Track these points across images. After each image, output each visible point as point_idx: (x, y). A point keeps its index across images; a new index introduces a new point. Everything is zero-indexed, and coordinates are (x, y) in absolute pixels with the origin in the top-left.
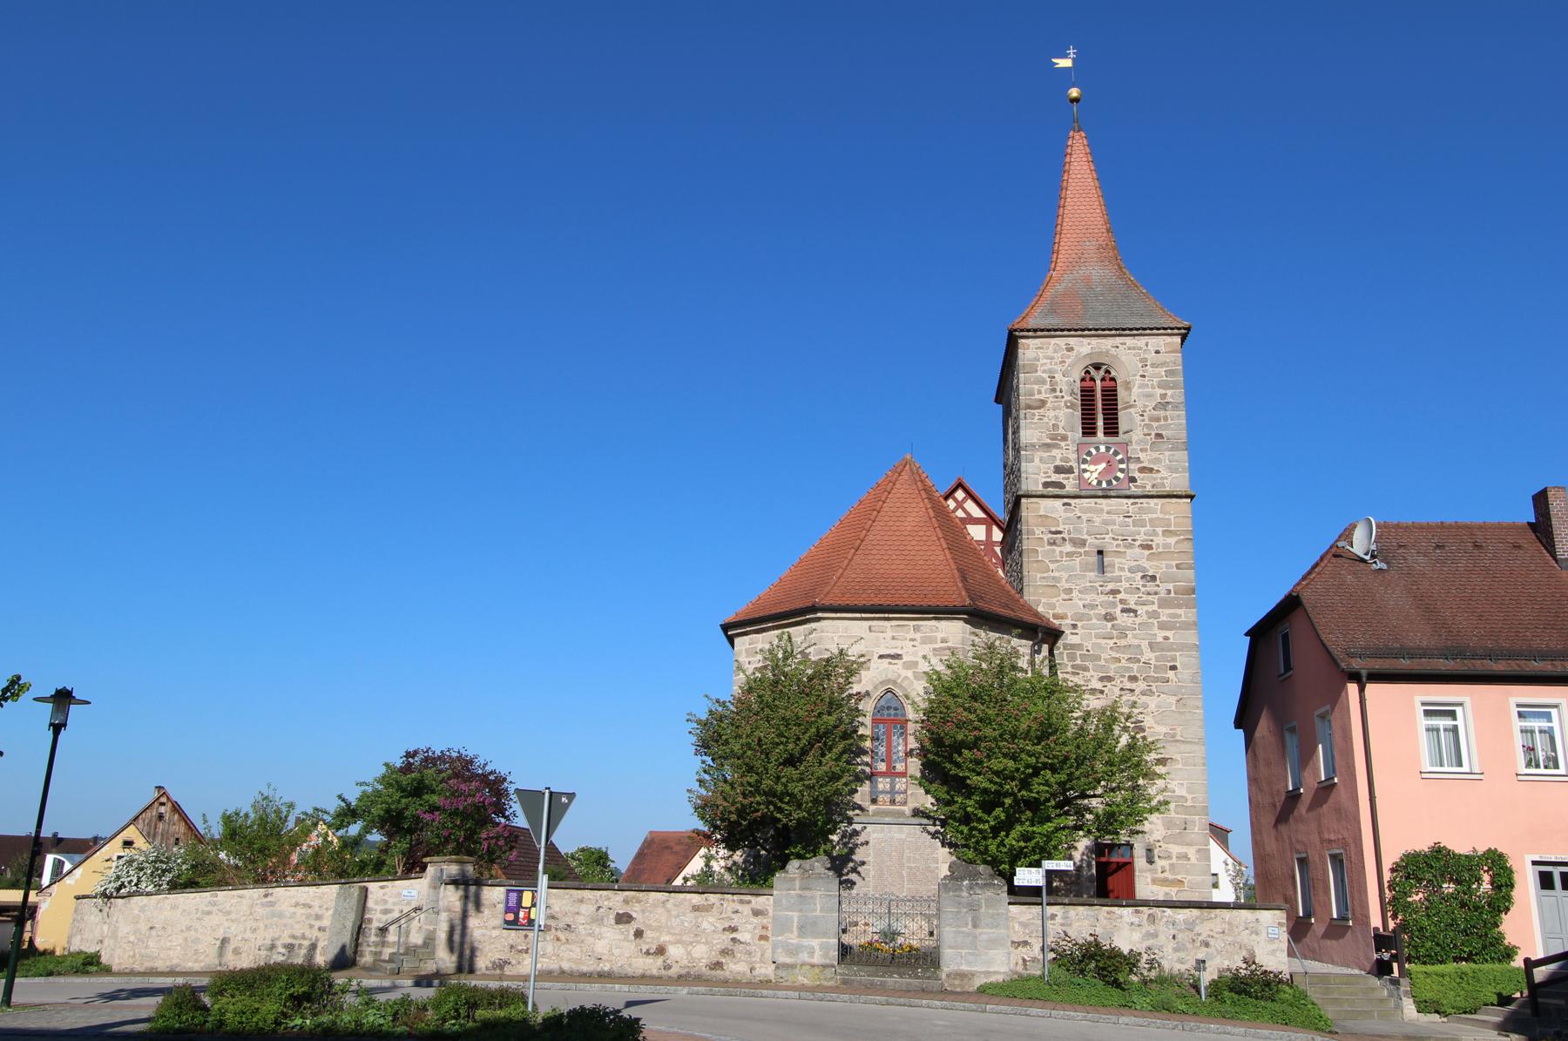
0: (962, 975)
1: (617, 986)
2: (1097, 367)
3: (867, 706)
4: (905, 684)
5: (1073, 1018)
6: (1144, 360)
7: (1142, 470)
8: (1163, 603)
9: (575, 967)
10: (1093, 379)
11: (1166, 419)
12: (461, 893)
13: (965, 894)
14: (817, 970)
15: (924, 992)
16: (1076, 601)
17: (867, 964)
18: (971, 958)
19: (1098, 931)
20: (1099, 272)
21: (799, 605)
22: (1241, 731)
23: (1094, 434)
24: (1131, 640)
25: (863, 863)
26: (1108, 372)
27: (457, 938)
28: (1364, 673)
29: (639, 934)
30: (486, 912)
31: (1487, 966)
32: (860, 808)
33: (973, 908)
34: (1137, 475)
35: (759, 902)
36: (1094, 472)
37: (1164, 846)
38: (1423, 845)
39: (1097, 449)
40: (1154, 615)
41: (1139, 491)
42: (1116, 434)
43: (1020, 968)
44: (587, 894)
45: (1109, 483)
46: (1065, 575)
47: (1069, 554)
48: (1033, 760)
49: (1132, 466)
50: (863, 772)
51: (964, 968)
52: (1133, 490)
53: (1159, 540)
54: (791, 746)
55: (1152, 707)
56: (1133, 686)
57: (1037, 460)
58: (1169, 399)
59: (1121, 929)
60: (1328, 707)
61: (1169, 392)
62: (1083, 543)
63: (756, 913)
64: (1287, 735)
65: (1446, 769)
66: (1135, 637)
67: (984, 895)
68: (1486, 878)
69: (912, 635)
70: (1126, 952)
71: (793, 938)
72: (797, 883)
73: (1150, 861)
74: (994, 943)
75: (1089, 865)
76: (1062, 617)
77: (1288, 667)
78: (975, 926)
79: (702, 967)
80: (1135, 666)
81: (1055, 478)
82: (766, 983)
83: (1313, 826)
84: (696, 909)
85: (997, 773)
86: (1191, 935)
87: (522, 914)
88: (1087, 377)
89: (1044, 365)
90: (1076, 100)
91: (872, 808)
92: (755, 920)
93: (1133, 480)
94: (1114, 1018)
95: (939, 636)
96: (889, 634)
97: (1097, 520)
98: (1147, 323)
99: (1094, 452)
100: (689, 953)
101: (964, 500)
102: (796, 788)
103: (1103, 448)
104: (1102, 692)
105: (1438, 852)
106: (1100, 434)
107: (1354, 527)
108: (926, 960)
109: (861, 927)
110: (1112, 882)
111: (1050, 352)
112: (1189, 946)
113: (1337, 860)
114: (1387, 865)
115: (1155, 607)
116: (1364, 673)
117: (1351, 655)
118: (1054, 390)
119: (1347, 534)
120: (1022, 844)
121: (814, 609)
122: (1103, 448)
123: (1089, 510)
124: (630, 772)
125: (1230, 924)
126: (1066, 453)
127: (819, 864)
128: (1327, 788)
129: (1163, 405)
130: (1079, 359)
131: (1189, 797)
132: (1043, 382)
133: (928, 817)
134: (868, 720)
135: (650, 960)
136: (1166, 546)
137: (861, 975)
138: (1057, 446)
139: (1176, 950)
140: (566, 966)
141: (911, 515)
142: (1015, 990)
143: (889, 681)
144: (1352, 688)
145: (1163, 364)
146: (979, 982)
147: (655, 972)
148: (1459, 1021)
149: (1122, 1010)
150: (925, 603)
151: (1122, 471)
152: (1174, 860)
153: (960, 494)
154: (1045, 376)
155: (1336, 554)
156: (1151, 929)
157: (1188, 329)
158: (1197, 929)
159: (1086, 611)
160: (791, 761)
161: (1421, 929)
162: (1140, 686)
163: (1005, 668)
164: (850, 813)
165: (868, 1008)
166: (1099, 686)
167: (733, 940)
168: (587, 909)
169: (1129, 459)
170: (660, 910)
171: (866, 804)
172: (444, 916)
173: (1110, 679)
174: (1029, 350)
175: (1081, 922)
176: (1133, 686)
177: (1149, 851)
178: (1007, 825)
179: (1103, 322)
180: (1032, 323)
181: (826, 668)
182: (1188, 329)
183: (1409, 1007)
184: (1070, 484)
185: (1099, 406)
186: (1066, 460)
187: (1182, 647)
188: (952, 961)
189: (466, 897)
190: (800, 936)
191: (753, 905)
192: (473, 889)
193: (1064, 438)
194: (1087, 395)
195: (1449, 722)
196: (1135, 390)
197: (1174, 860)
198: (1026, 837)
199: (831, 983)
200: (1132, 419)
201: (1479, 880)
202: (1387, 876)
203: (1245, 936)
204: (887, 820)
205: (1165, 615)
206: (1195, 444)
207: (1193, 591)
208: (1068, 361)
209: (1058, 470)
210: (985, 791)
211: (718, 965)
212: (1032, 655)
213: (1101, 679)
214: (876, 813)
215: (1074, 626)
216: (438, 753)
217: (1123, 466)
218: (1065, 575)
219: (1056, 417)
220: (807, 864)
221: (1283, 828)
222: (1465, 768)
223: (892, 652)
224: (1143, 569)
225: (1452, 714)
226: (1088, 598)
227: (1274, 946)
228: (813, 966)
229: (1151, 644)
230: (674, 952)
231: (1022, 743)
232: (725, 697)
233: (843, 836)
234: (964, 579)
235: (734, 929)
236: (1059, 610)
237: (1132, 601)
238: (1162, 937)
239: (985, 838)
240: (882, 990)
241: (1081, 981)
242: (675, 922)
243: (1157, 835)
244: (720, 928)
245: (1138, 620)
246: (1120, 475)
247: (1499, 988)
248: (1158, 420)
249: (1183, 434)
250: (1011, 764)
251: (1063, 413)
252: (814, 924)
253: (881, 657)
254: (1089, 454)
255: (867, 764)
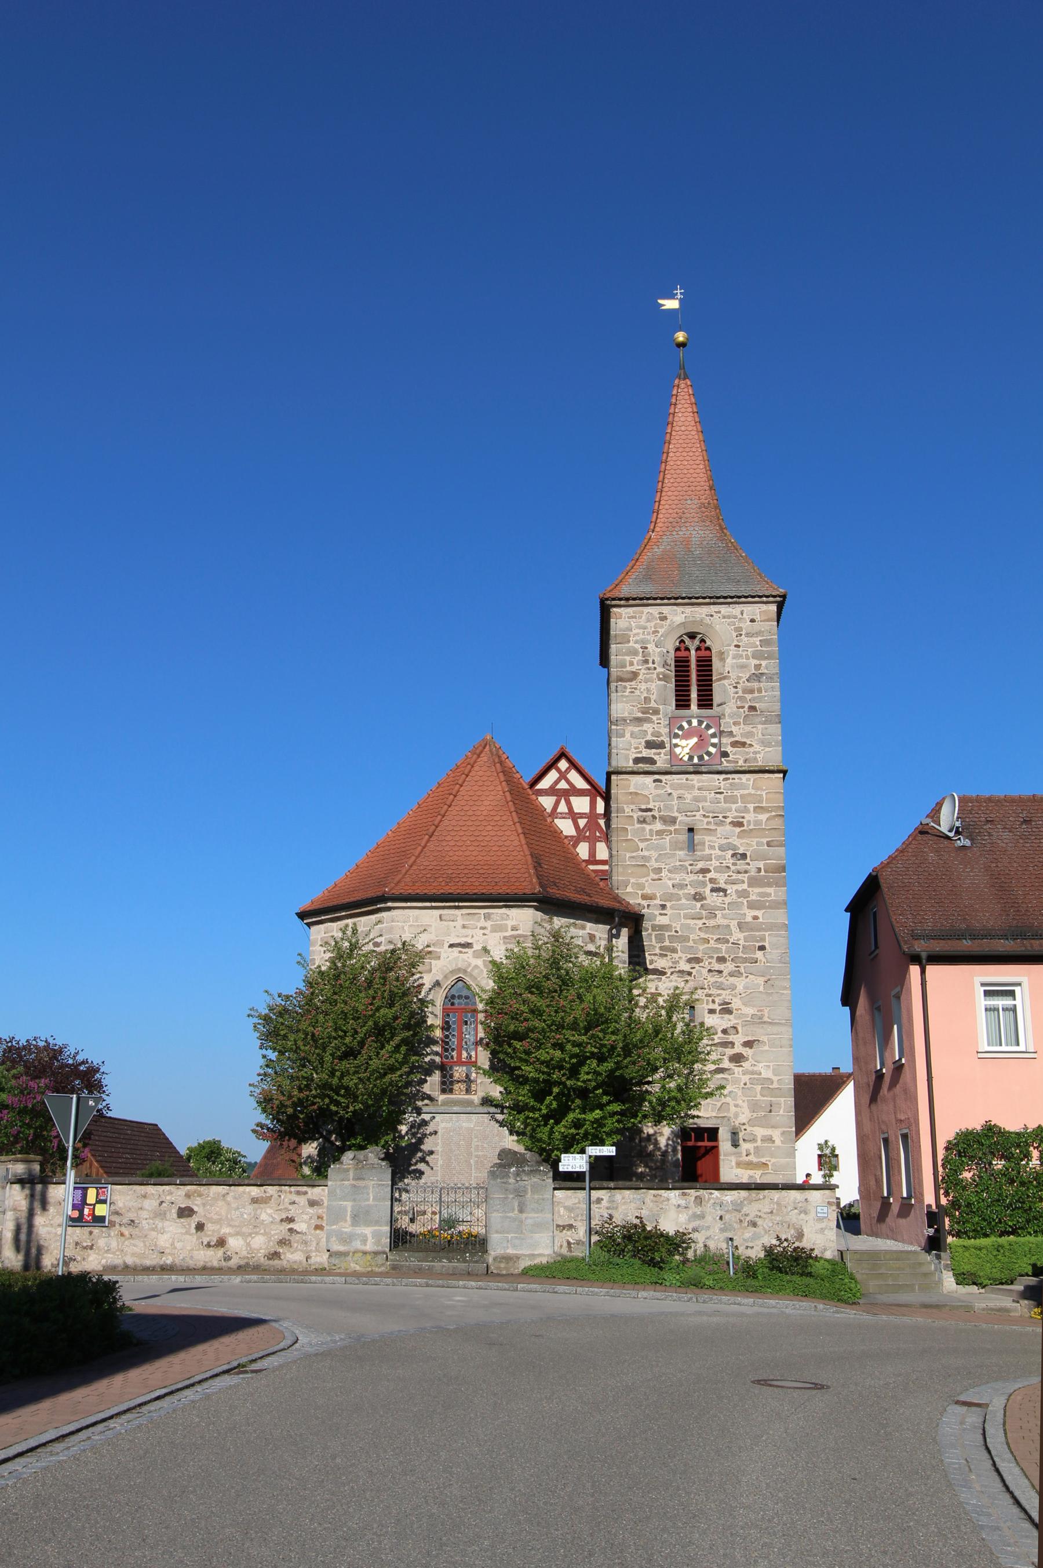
0: (508, 1259)
1: (173, 1277)
2: (692, 636)
3: (439, 998)
4: (475, 973)
5: (597, 1294)
6: (738, 630)
7: (735, 744)
8: (754, 882)
9: (138, 1261)
10: (687, 649)
11: (760, 691)
12: (27, 1191)
13: (512, 1180)
14: (369, 1257)
15: (469, 1275)
16: (665, 880)
17: (427, 1250)
18: (517, 1242)
19: (644, 1213)
20: (699, 533)
21: (370, 894)
22: (847, 1008)
23: (688, 706)
24: (720, 920)
25: (431, 1153)
26: (703, 641)
27: (23, 1237)
28: (924, 955)
29: (200, 1227)
30: (52, 1210)
31: (1028, 1238)
32: (430, 1098)
33: (520, 1194)
34: (729, 749)
35: (315, 1193)
36: (685, 747)
37: (749, 1129)
38: (976, 1124)
39: (689, 723)
40: (743, 894)
41: (730, 766)
42: (710, 706)
43: (564, 1251)
44: (150, 1189)
45: (701, 758)
46: (654, 854)
47: (660, 833)
48: (577, 1050)
49: (724, 740)
50: (433, 1061)
51: (510, 1251)
52: (725, 764)
53: (750, 817)
54: (347, 1040)
55: (740, 987)
56: (721, 967)
57: (628, 735)
58: (763, 670)
59: (669, 1210)
60: (898, 989)
61: (764, 663)
62: (673, 821)
63: (312, 1203)
64: (876, 1013)
65: (1004, 1048)
66: (724, 917)
67: (529, 1182)
68: (1035, 1154)
69: (482, 923)
70: (672, 1233)
71: (347, 1228)
72: (351, 1174)
73: (735, 1144)
74: (538, 1227)
75: (675, 1150)
76: (651, 897)
77: (876, 947)
78: (521, 1211)
79: (260, 1257)
80: (724, 947)
81: (646, 753)
82: (321, 1271)
83: (891, 1106)
84: (255, 1201)
85: (547, 1063)
86: (739, 1216)
87: (86, 1211)
88: (681, 648)
89: (636, 635)
90: (682, 345)
91: (442, 1097)
92: (311, 1210)
93: (725, 754)
94: (634, 1293)
95: (510, 923)
96: (460, 922)
97: (688, 797)
98: (743, 590)
99: (685, 725)
100: (248, 1244)
101: (568, 770)
102: (351, 1082)
103: (695, 722)
104: (690, 974)
105: (990, 1129)
106: (694, 706)
107: (944, 799)
108: (477, 1244)
109: (429, 1215)
110: (702, 1166)
111: (642, 622)
112: (736, 1226)
113: (905, 1137)
114: (941, 1145)
115: (745, 886)
116: (924, 955)
117: (916, 937)
118: (646, 662)
119: (935, 814)
120: (573, 1131)
121: (383, 899)
122: (695, 722)
123: (680, 786)
124: (192, 1063)
125: (778, 1204)
126: (657, 727)
127: (373, 1155)
128: (898, 1068)
129: (757, 677)
130: (672, 629)
131: (775, 1079)
132: (635, 653)
133: (496, 1106)
134: (438, 1010)
135: (210, 1252)
136: (757, 822)
137: (410, 1259)
138: (648, 720)
139: (722, 1230)
140: (130, 1260)
141: (487, 795)
142: (559, 1271)
143: (459, 970)
144: (914, 970)
145: (758, 633)
146: (524, 1264)
147: (215, 1264)
148: (993, 1291)
149: (803, 1299)
150: (495, 891)
151: (714, 745)
152: (759, 1143)
153: (563, 765)
154: (638, 646)
155: (923, 831)
156: (698, 1211)
157: (784, 597)
158: (745, 1210)
159: (676, 891)
160: (350, 1053)
161: (969, 1205)
162: (728, 967)
163: (559, 953)
164: (419, 1103)
165: (415, 1291)
166: (686, 967)
167: (291, 1230)
168: (150, 1204)
169: (721, 732)
170: (220, 1203)
171: (436, 1093)
172: (10, 1215)
173: (698, 960)
174: (622, 619)
175: (625, 1206)
176: (721, 967)
177: (734, 1134)
178: (558, 1115)
179: (698, 589)
180: (625, 590)
181: (390, 962)
182: (784, 597)
183: (949, 1281)
184: (662, 760)
185: (693, 677)
186: (657, 734)
187: (771, 927)
188: (499, 1246)
189: (32, 1196)
190: (353, 1225)
191: (309, 1196)
192: (39, 1187)
193: (656, 712)
194: (681, 665)
195: (1008, 1002)
196: (729, 661)
197: (759, 1143)
198: (577, 1124)
199: (383, 1269)
200: (725, 691)
201: (1027, 1156)
202: (941, 1154)
203: (794, 1217)
204: (455, 1109)
205: (755, 894)
206: (787, 718)
207: (783, 869)
208: (661, 631)
209: (650, 745)
210: (536, 1081)
211: (276, 1255)
212: (610, 940)
213: (689, 961)
214: (445, 1103)
215: (663, 907)
216: (23, 1042)
217: (715, 740)
218: (654, 854)
219: (648, 690)
220: (361, 1154)
221: (873, 1106)
222: (1021, 1048)
223: (462, 940)
224: (735, 848)
225: (1012, 994)
226: (678, 878)
227: (823, 1225)
228: (365, 1253)
229: (740, 926)
230: (234, 1243)
231: (568, 1034)
232: (292, 992)
233: (412, 1126)
234: (538, 864)
235: (291, 1220)
236: (648, 891)
237: (722, 879)
238: (709, 1218)
239: (539, 1126)
240: (430, 1273)
241: (619, 1261)
242: (235, 1214)
243: (743, 1119)
244: (278, 1219)
245: (727, 900)
246: (712, 750)
247: (1033, 1260)
248: (752, 692)
249: (777, 707)
250: (558, 1054)
251: (656, 685)
252: (367, 1213)
253: (451, 946)
254: (681, 728)
255: (437, 1054)
